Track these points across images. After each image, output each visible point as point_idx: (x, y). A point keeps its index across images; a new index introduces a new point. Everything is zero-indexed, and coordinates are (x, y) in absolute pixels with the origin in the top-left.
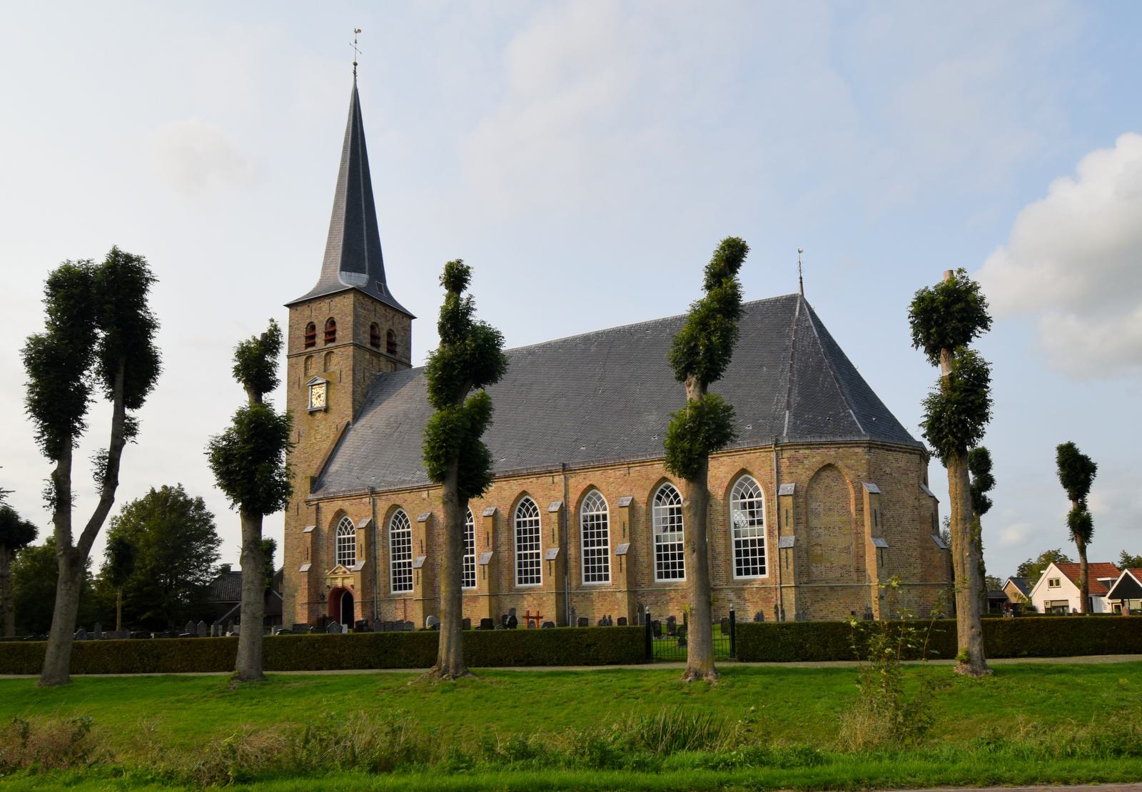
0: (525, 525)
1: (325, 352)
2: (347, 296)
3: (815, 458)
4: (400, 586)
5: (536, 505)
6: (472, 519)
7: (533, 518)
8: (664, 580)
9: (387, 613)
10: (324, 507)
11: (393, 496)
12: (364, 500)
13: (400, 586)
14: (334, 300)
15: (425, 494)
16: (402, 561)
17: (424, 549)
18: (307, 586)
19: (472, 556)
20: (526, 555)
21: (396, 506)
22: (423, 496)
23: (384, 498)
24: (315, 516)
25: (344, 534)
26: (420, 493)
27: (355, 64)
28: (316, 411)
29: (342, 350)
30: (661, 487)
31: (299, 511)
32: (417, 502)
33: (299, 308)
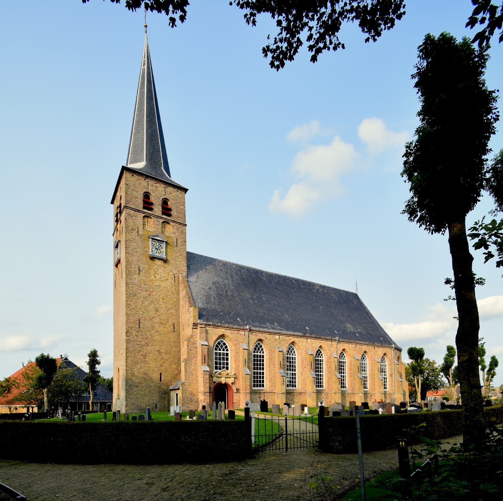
0: (257, 357)
1: (145, 215)
2: (179, 191)
3: (254, 338)
4: (257, 385)
5: (227, 344)
6: (228, 349)
7: (225, 352)
8: (256, 388)
9: (254, 400)
10: (210, 331)
11: (260, 334)
12: (240, 332)
13: (257, 385)
14: (169, 188)
15: (277, 337)
16: (259, 371)
17: (282, 366)
18: (208, 381)
19: (263, 371)
20: (257, 372)
21: (260, 340)
22: (276, 338)
23: (253, 334)
24: (205, 335)
25: (220, 350)
26: (274, 336)
27: (146, 26)
28: (156, 258)
29: (178, 226)
30: (219, 341)
31: (141, 325)
32: (273, 340)
33: (135, 175)
